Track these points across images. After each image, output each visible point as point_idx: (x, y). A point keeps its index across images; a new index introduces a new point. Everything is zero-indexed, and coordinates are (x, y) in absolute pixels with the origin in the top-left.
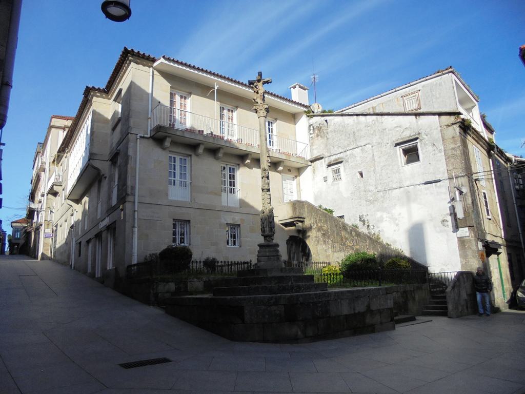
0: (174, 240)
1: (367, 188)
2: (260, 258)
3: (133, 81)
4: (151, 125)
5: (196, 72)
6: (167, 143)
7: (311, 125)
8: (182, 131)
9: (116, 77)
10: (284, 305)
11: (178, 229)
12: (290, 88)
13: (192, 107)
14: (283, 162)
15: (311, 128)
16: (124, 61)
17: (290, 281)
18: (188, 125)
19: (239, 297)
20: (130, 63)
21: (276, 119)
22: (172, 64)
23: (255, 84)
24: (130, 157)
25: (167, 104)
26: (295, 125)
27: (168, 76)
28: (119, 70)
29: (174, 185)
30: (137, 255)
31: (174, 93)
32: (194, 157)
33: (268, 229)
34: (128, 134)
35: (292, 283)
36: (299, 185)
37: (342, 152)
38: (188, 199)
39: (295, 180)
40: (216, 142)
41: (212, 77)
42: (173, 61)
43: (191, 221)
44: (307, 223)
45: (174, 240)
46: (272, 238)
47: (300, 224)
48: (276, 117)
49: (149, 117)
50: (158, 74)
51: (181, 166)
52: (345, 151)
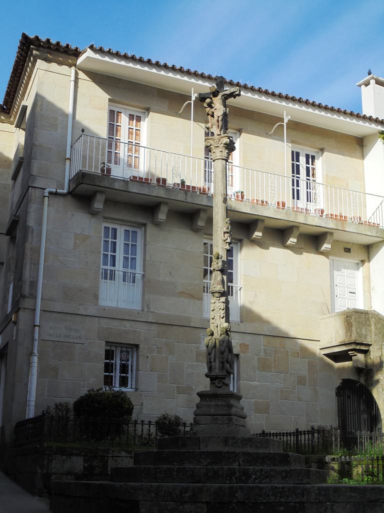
0: (108, 381)
2: (198, 417)
3: (40, 93)
4: (70, 171)
5: (154, 71)
6: (98, 205)
8: (125, 182)
9: (18, 85)
10: (207, 503)
11: (117, 362)
12: (360, 86)
13: (151, 137)
14: (332, 234)
16: (25, 63)
17: (235, 462)
18: (143, 168)
19: (134, 484)
20: (35, 61)
21: (322, 150)
22: (107, 59)
23: (208, 100)
24: (31, 229)
25: (102, 130)
26: (363, 160)
27: (101, 79)
28: (21, 73)
30: (36, 406)
31: (116, 110)
32: (151, 229)
33: (217, 365)
34: (29, 188)
35: (239, 465)
36: (367, 279)
38: (137, 307)
39: (361, 268)
40: (189, 200)
41: (186, 78)
42: (110, 53)
43: (141, 346)
44: (375, 355)
45: (108, 381)
46: (226, 381)
47: (360, 357)
48: (321, 147)
49: (68, 156)
50: (86, 77)
51: (126, 245)
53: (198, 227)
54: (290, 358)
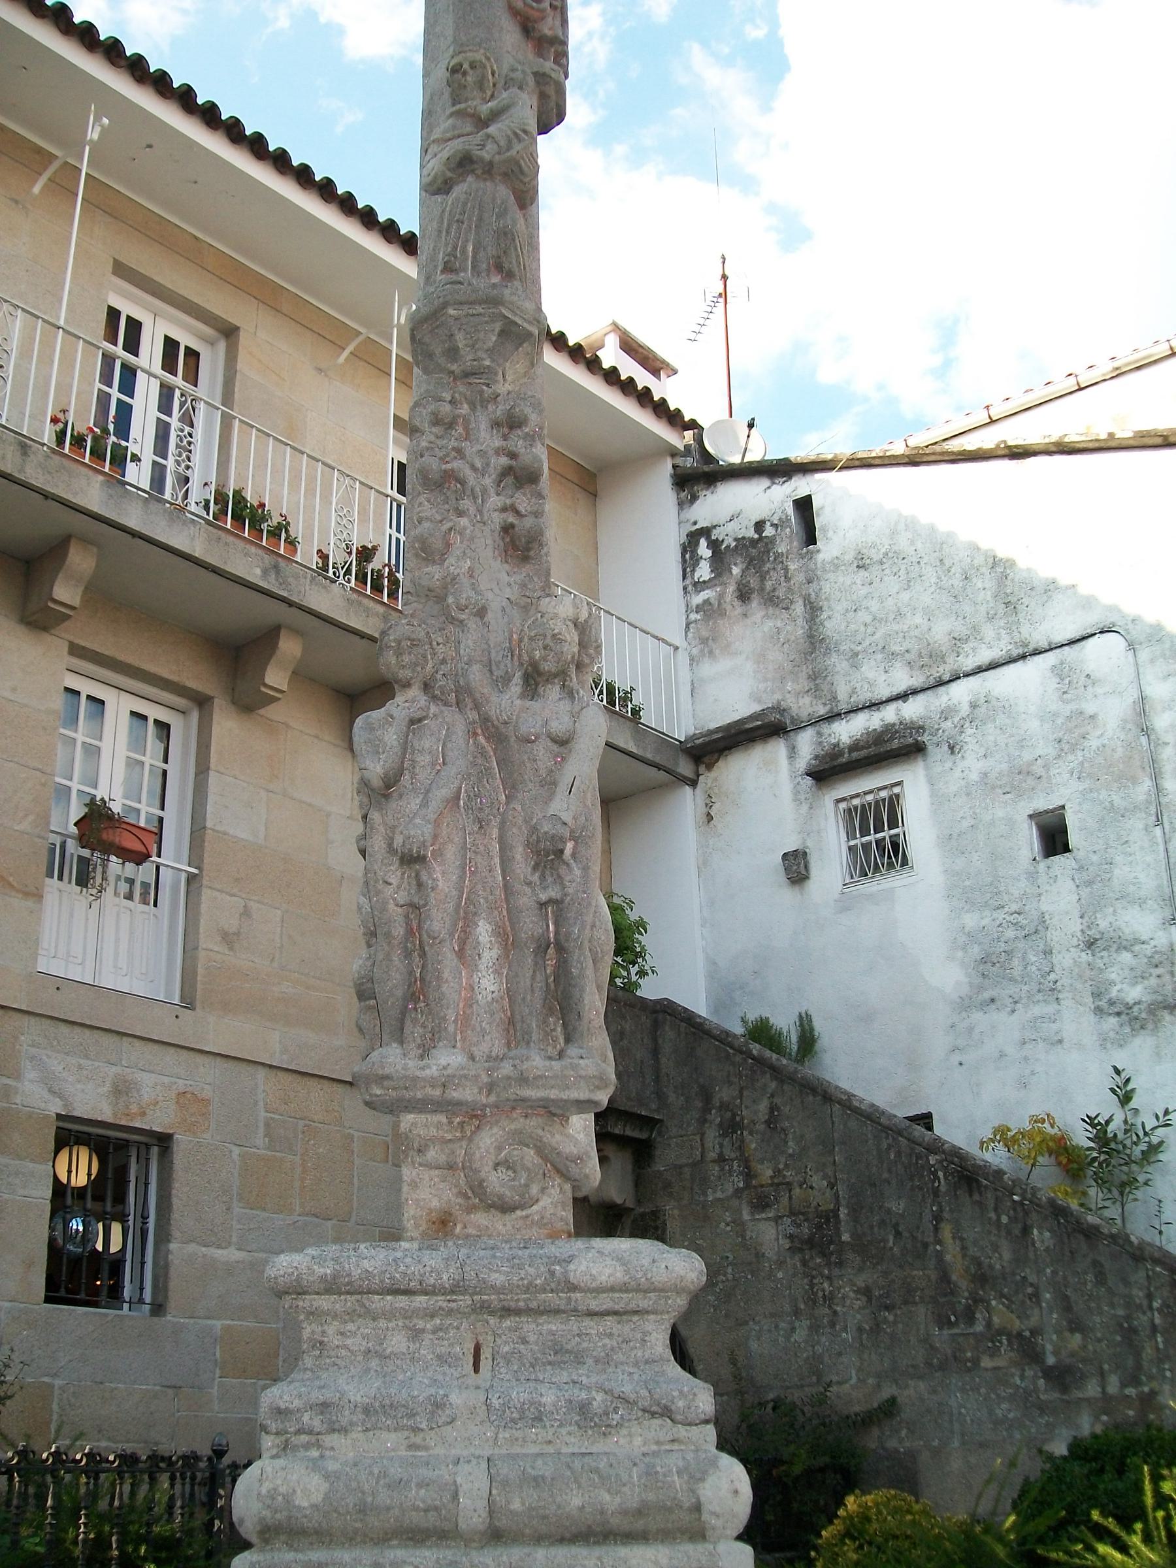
1: (1103, 924)
7: (705, 532)
15: (704, 550)
29: (155, 905)
33: (488, 985)
37: (915, 692)
52: (941, 683)
53: (51, 605)
54: (357, 1161)
